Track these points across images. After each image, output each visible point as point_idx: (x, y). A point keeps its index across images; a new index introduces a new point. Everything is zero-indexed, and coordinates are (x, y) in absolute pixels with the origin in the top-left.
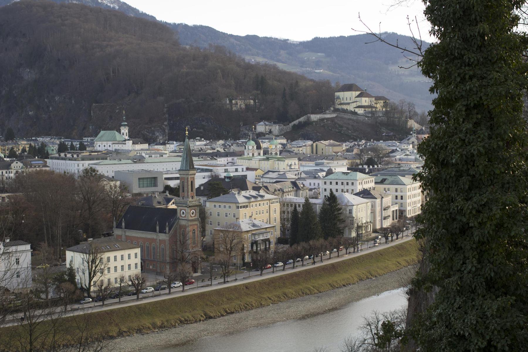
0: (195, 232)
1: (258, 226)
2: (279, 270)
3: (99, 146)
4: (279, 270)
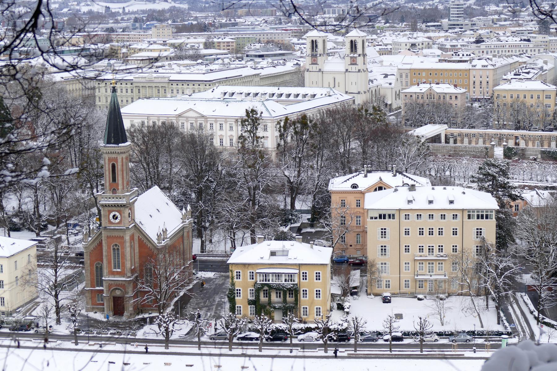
0: (118, 249)
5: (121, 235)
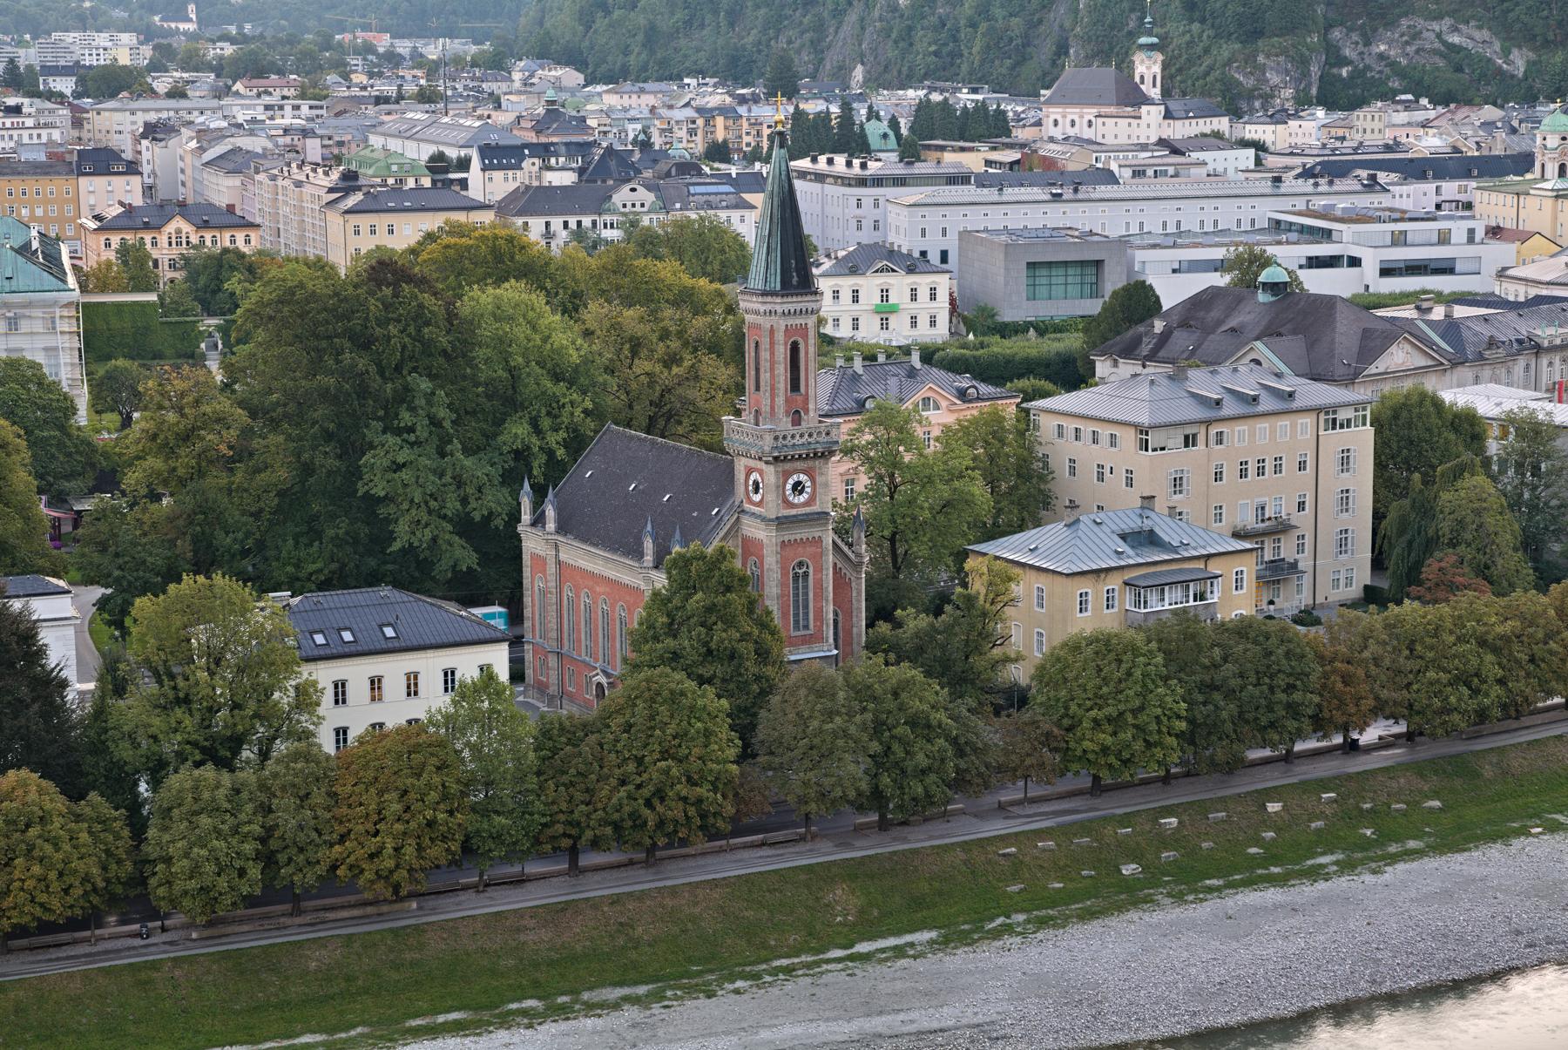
0: (806, 575)
1: (1174, 550)
2: (1145, 782)
3: (1056, 123)
4: (1145, 782)
5: (817, 535)
